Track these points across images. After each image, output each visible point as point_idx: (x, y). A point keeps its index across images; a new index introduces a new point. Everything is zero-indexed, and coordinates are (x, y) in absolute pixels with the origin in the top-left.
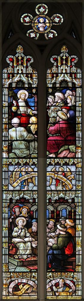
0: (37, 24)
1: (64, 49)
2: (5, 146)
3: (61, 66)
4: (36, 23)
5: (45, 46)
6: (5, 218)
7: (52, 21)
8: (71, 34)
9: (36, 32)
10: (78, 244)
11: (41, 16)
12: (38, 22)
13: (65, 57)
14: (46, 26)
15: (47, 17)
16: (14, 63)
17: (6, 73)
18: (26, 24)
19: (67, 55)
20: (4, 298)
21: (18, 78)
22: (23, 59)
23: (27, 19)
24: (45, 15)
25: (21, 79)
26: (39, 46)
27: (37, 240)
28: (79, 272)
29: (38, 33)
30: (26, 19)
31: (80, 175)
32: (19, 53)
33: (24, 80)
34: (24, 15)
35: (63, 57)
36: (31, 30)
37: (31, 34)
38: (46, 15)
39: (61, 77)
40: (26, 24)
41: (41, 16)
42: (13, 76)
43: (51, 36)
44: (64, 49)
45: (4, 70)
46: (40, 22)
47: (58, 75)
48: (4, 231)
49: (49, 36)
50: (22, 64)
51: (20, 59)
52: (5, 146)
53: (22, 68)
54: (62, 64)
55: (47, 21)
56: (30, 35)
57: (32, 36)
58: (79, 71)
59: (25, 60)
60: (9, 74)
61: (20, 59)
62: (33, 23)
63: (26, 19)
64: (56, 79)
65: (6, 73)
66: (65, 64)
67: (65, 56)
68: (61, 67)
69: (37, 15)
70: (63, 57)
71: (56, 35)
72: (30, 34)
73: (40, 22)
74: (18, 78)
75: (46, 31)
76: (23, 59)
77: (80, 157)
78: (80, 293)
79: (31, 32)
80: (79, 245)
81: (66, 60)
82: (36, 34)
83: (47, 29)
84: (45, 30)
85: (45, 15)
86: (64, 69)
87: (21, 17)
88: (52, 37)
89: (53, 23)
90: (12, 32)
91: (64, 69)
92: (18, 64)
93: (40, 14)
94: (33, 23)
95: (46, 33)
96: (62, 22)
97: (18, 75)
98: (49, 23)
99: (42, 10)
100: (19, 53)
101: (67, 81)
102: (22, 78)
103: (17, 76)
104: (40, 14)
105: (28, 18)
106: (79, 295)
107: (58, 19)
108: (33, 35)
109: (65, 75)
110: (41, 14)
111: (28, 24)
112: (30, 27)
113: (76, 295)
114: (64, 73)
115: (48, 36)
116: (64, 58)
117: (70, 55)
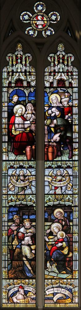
0: (36, 22)
1: (61, 47)
2: (4, 147)
3: (16, 65)
4: (35, 20)
5: (42, 44)
6: (76, 226)
7: (49, 18)
8: (67, 32)
9: (35, 30)
10: (75, 250)
11: (39, 14)
12: (36, 20)
13: (20, 56)
14: (44, 23)
15: (45, 15)
16: (14, 61)
17: (6, 72)
18: (25, 22)
19: (64, 53)
20: (4, 306)
21: (60, 77)
22: (64, 56)
23: (26, 17)
24: (43, 13)
25: (62, 77)
26: (37, 44)
27: (35, 245)
28: (76, 279)
29: (36, 30)
30: (25, 17)
31: (75, 176)
32: (60, 51)
33: (22, 78)
34: (24, 13)
35: (60, 56)
36: (30, 28)
37: (30, 31)
38: (44, 13)
39: (16, 76)
40: (25, 22)
41: (39, 14)
42: (13, 75)
43: (48, 33)
44: (61, 47)
45: (4, 69)
46: (38, 20)
47: (55, 74)
48: (4, 236)
49: (47, 34)
50: (21, 63)
51: (19, 59)
52: (4, 147)
53: (63, 67)
54: (17, 63)
55: (45, 19)
56: (28, 32)
57: (30, 34)
58: (75, 70)
59: (66, 58)
60: (8, 73)
61: (19, 59)
62: (32, 20)
63: (25, 17)
64: (12, 78)
65: (6, 72)
66: (20, 63)
67: (62, 55)
68: (16, 66)
69: (36, 13)
70: (60, 56)
71: (53, 33)
72: (29, 31)
73: (38, 20)
74: (60, 77)
75: (45, 28)
76: (64, 56)
77: (76, 159)
78: (76, 300)
79: (30, 30)
80: (76, 251)
81: (63, 60)
82: (34, 32)
83: (45, 26)
84: (43, 27)
85: (43, 13)
86: (61, 68)
87: (20, 15)
88: (49, 34)
89: (50, 21)
90: (12, 30)
91: (61, 68)
92: (17, 62)
93: (38, 12)
94: (32, 20)
95: (44, 30)
96: (59, 19)
97: (59, 74)
98: (47, 21)
99: (40, 8)
100: (18, 51)
101: (22, 79)
102: (21, 77)
103: (58, 75)
104: (38, 12)
105: (27, 16)
106: (76, 302)
107: (55, 17)
108: (31, 33)
109: (62, 73)
110: (39, 12)
111: (27, 22)
112: (29, 25)
113: (73, 302)
114: (19, 72)
115: (46, 34)
116: (61, 56)
117: (67, 54)
